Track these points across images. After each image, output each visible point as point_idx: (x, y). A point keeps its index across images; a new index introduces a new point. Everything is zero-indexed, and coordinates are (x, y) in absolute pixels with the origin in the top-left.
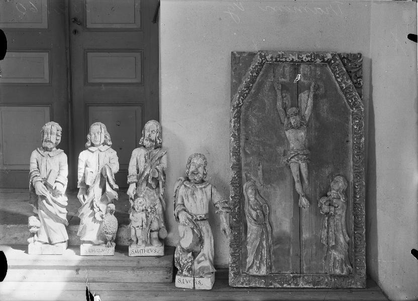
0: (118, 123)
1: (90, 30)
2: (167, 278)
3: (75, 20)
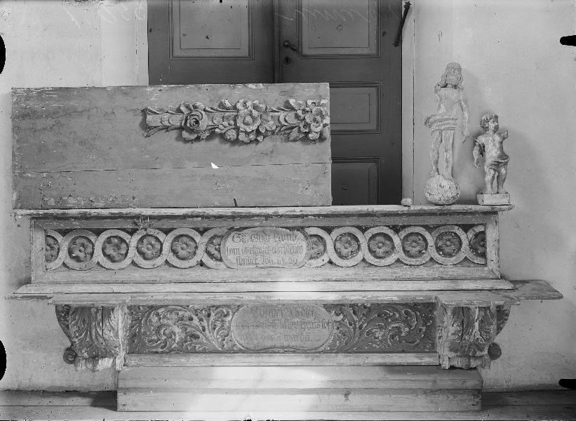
1: (305, 56)
2: (473, 405)
3: (289, 46)
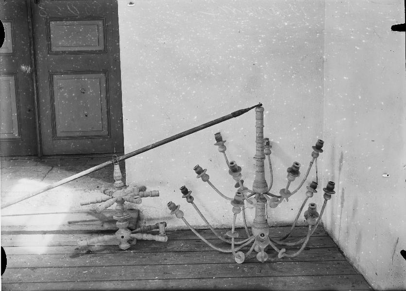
0: (83, 91)
